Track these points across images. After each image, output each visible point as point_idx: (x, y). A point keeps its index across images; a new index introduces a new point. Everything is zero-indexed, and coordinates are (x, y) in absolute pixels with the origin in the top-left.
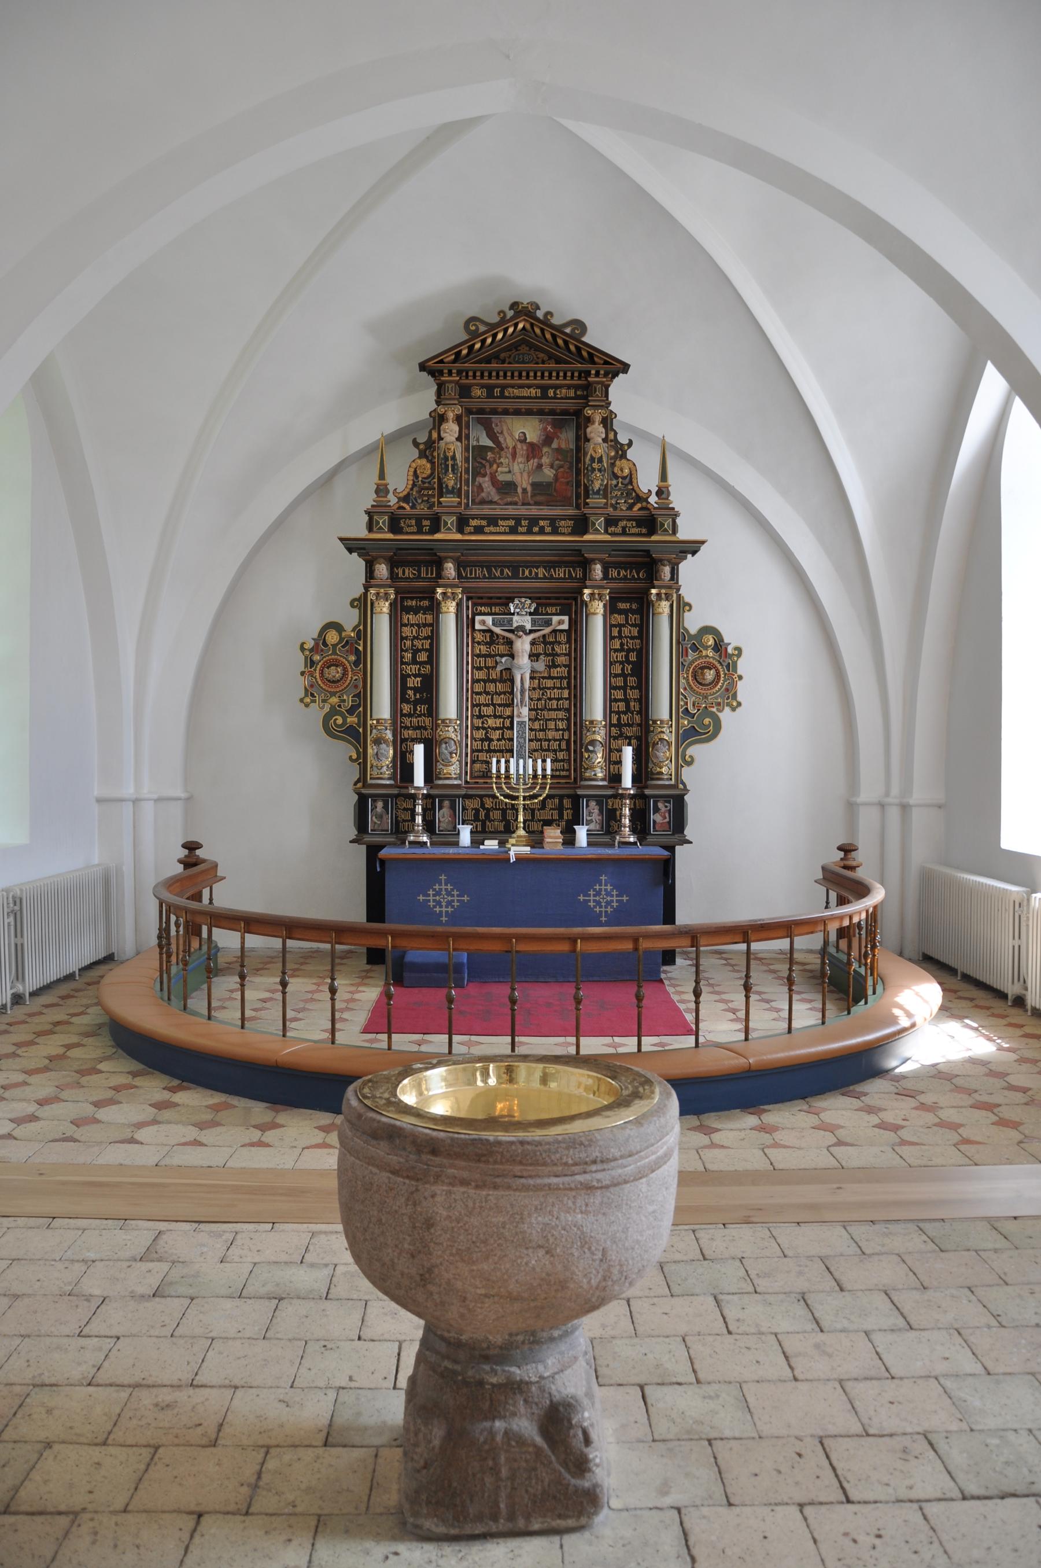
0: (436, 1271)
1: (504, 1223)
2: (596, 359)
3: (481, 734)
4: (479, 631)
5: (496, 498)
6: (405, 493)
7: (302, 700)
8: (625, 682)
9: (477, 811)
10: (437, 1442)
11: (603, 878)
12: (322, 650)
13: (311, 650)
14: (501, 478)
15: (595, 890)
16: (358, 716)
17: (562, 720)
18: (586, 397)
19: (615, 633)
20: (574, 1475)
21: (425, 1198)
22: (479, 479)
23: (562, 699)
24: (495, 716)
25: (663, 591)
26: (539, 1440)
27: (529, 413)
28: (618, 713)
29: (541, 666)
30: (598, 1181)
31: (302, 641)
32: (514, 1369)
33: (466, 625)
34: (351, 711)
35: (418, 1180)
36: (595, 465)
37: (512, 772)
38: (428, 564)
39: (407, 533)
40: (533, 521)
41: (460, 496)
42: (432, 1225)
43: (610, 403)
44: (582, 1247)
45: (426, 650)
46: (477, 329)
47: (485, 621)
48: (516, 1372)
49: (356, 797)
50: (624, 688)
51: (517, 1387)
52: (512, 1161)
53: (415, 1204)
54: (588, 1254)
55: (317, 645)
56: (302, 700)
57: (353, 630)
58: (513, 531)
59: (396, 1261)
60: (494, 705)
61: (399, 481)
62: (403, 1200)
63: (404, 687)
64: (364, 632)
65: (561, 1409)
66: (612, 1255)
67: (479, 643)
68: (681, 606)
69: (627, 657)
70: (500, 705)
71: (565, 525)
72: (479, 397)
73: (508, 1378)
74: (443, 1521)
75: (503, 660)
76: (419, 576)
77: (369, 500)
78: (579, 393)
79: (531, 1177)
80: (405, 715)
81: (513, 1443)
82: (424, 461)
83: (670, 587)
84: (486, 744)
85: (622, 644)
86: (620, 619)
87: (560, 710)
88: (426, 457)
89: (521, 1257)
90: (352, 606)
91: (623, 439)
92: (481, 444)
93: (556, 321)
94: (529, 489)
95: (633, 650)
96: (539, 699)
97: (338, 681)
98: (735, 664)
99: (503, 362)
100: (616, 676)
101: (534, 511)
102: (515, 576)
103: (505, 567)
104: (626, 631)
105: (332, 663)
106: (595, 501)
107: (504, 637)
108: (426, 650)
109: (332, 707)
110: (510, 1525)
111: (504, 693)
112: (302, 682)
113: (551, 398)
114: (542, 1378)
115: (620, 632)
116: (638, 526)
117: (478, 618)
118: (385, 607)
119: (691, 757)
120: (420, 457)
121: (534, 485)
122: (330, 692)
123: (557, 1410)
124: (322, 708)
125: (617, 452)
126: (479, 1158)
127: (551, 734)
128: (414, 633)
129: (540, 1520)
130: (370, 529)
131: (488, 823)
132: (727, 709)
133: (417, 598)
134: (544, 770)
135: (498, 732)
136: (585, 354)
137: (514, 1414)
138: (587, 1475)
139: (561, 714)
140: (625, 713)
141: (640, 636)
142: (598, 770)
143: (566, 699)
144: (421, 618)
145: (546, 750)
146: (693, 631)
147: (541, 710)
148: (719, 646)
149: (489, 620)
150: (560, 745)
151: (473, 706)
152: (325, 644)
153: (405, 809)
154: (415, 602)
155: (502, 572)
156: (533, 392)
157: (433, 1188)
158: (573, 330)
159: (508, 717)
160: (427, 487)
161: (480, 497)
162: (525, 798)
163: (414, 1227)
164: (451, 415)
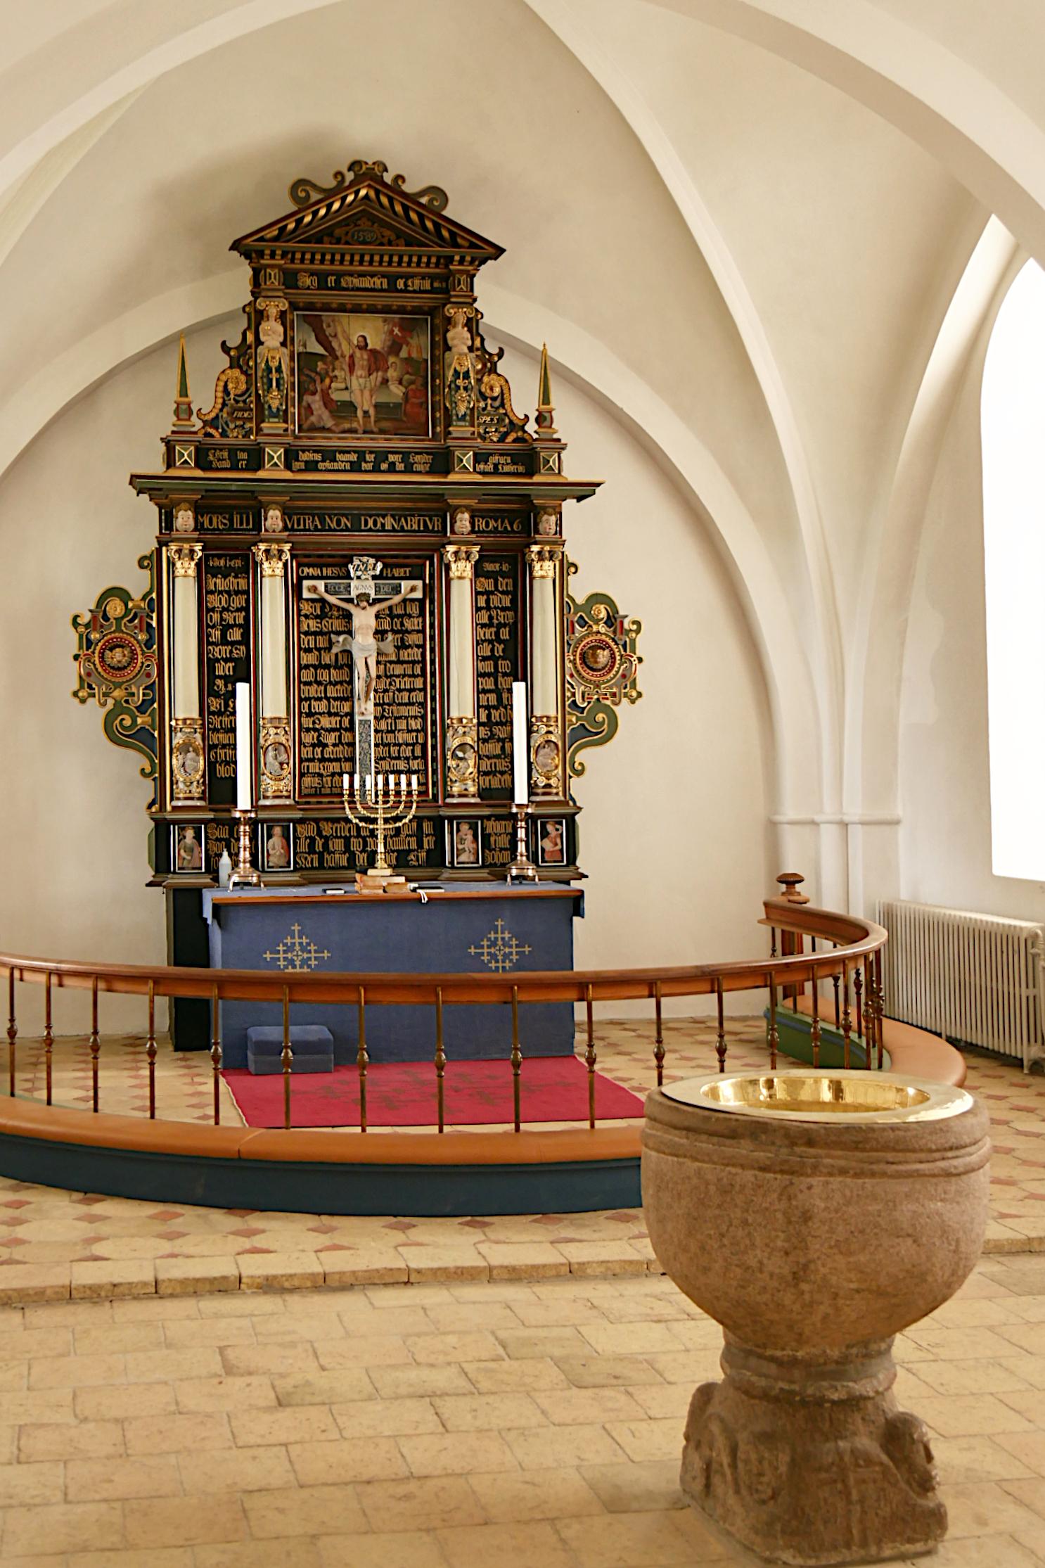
0: (812, 1266)
1: (879, 1211)
2: (459, 240)
3: (309, 738)
4: (307, 600)
5: (329, 423)
6: (213, 415)
7: (75, 694)
8: (496, 666)
9: (312, 840)
10: (783, 1469)
11: (499, 923)
12: (102, 626)
13: (87, 626)
14: (336, 396)
15: (489, 939)
16: (152, 715)
17: (416, 717)
18: (446, 291)
19: (482, 603)
20: (919, 1494)
21: (801, 1191)
22: (308, 398)
23: (414, 690)
24: (330, 714)
25: (547, 548)
26: (885, 1458)
27: (372, 310)
28: (488, 708)
29: (389, 644)
30: (955, 1167)
31: (77, 612)
32: (851, 1384)
33: (294, 591)
34: (142, 709)
35: (792, 1173)
36: (460, 382)
37: (368, 787)
38: (241, 510)
39: (218, 470)
40: (382, 455)
41: (286, 422)
42: (810, 1218)
43: (475, 300)
44: (942, 1236)
45: (240, 626)
46: (308, 196)
47: (315, 587)
48: (859, 1388)
49: (152, 824)
50: (494, 675)
51: (855, 1403)
52: (886, 1148)
53: (789, 1199)
54: (946, 1245)
55: (94, 618)
56: (75, 694)
57: (143, 599)
58: (355, 467)
59: (765, 1261)
60: (328, 699)
61: (205, 399)
62: (775, 1196)
63: (213, 676)
64: (156, 601)
65: (899, 1425)
66: (963, 1248)
67: (306, 617)
68: (566, 568)
69: (497, 634)
70: (335, 699)
71: (420, 461)
72: (308, 288)
73: (848, 1393)
74: (800, 1552)
75: (341, 638)
76: (231, 528)
77: (167, 424)
78: (436, 285)
79: (900, 1163)
80: (213, 713)
81: (861, 1462)
82: (237, 372)
83: (555, 543)
84: (319, 750)
85: (490, 618)
86: (488, 584)
87: (413, 704)
88: (240, 367)
89: (893, 1247)
90: (141, 566)
91: (492, 348)
92: (309, 350)
93: (408, 188)
94: (372, 412)
95: (505, 625)
96: (386, 691)
97: (125, 668)
98: (633, 641)
99: (338, 242)
100: (485, 659)
101: (381, 443)
102: (356, 528)
103: (343, 515)
104: (495, 601)
105: (116, 642)
106: (459, 430)
107: (339, 608)
108: (240, 626)
109: (117, 703)
110: (862, 1552)
111: (341, 683)
112: (73, 671)
113: (401, 291)
114: (877, 1392)
115: (488, 601)
116: (514, 463)
117: (306, 583)
118: (186, 569)
119: (581, 764)
120: (231, 367)
121: (377, 406)
122: (113, 683)
123: (895, 1427)
124: (104, 705)
125: (484, 365)
126: (856, 1146)
127: (401, 737)
128: (223, 603)
129: (890, 1545)
130: (170, 463)
131: (326, 855)
132: (625, 701)
133: (225, 555)
134: (409, 784)
135: (333, 734)
136: (445, 234)
137: (854, 1434)
138: (930, 1494)
139: (415, 710)
140: (496, 707)
141: (513, 607)
142: (470, 782)
143: (420, 690)
144: (232, 582)
145: (396, 758)
146: (580, 600)
147: (389, 705)
148: (613, 620)
149: (321, 585)
150: (413, 751)
151: (301, 700)
152: (106, 618)
153: (217, 840)
154: (228, 563)
155: (339, 523)
156: (377, 282)
157: (809, 1180)
158: (431, 201)
159: (346, 715)
160: (244, 405)
161: (309, 422)
162: (386, 821)
163: (790, 1222)
164: (273, 312)
